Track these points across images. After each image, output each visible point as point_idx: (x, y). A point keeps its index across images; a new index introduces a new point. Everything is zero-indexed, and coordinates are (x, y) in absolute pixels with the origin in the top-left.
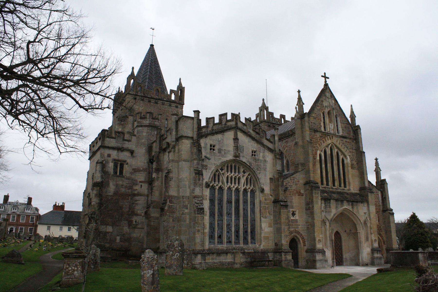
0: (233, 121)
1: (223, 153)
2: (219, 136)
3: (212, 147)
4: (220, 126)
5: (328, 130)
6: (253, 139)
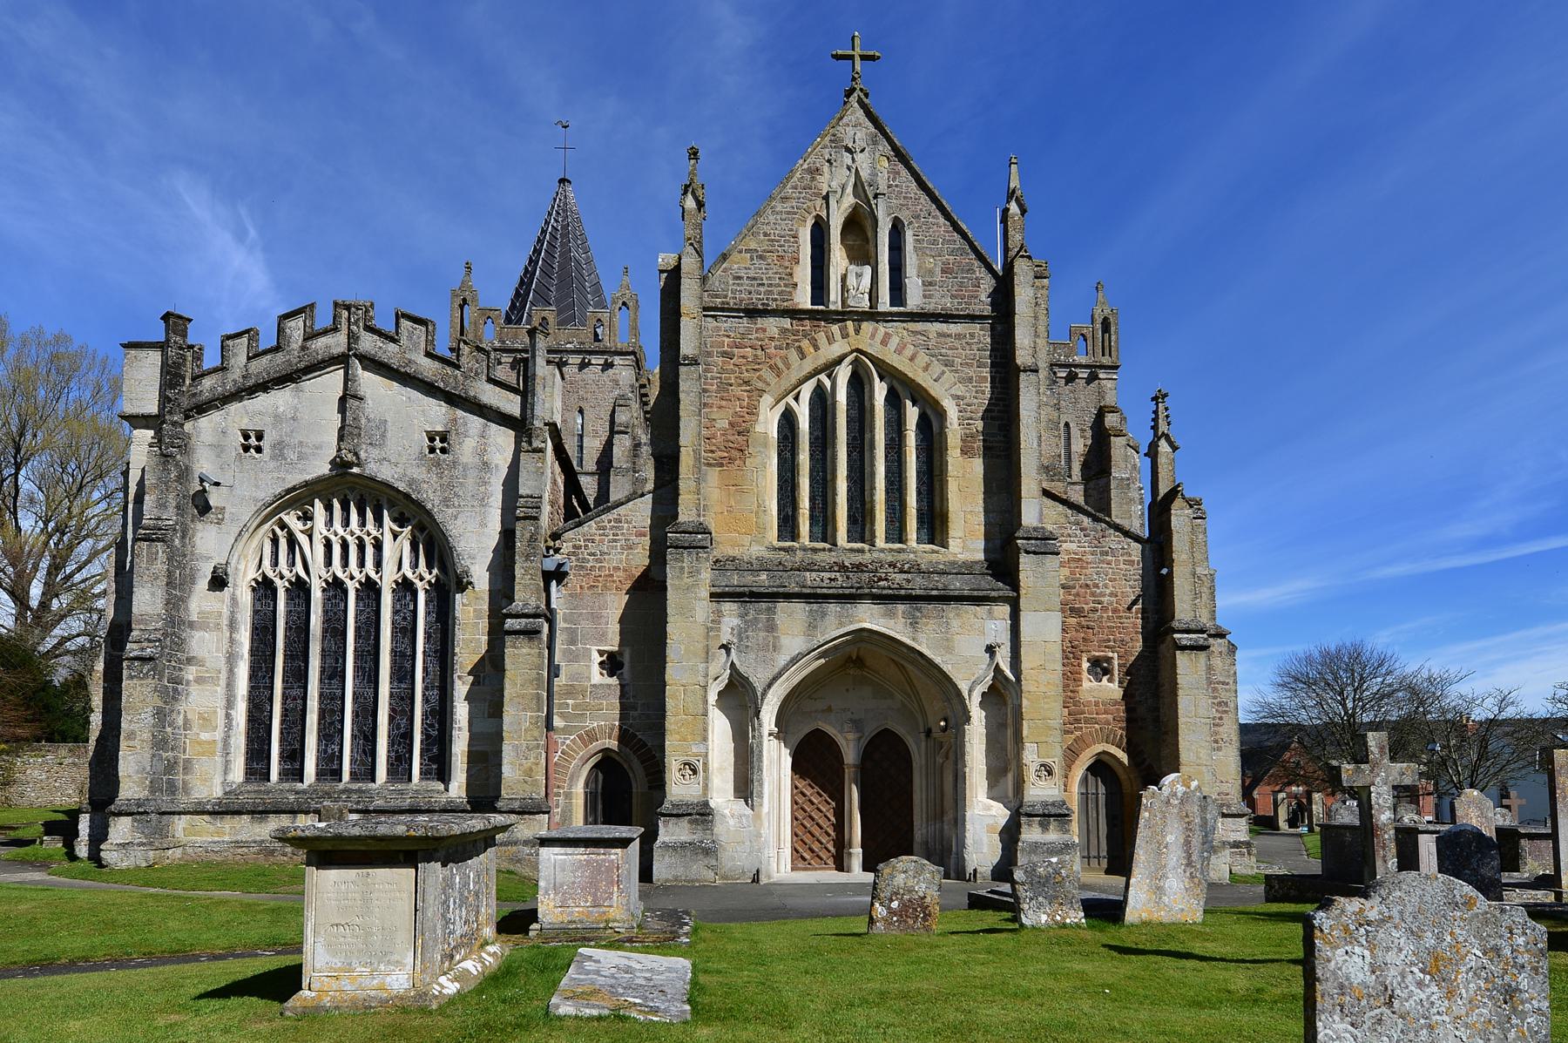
0: (335, 330)
1: (292, 455)
2: (280, 399)
3: (252, 441)
4: (280, 358)
6: (429, 389)
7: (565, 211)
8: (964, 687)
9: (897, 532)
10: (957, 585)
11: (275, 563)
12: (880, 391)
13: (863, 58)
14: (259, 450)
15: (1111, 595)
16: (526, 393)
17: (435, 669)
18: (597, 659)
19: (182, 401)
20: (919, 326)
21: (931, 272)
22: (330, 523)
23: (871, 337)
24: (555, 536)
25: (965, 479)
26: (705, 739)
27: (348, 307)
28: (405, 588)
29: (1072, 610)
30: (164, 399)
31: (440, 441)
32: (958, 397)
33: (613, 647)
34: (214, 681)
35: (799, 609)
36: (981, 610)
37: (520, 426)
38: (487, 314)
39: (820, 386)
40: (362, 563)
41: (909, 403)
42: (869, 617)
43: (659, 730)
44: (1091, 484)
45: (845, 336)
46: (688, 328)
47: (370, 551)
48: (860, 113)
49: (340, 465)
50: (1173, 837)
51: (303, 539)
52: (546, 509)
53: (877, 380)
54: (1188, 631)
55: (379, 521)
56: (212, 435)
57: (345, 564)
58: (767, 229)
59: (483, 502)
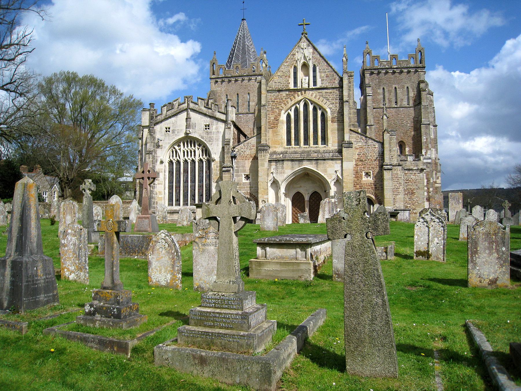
0: (185, 103)
1: (176, 132)
2: (173, 119)
3: (168, 130)
5: (385, 172)
6: (205, 115)
7: (243, 29)
8: (329, 181)
9: (316, 143)
10: (327, 155)
11: (173, 156)
12: (311, 107)
13: (306, 25)
14: (169, 131)
15: (371, 156)
16: (226, 114)
17: (208, 181)
18: (244, 176)
19: (154, 121)
20: (320, 91)
21: (323, 77)
22: (184, 147)
23: (309, 95)
24: (234, 148)
25: (332, 127)
26: (268, 195)
27: (186, 97)
28: (201, 161)
29: (360, 160)
30: (150, 123)
31: (207, 127)
32: (330, 108)
33: (248, 173)
34: (162, 184)
35: (290, 163)
36: (334, 162)
37: (225, 122)
38: (220, 67)
39: (296, 107)
40: (191, 156)
41: (318, 110)
42: (307, 165)
43: (257, 192)
44: (416, 107)
45: (302, 94)
46: (263, 97)
47: (193, 153)
48: (305, 39)
49: (187, 134)
50: (327, 209)
51: (179, 151)
52: (232, 141)
53: (310, 104)
54: (387, 165)
55: (195, 146)
56: (159, 129)
57: (188, 156)
58: (282, 70)
59: (217, 140)
